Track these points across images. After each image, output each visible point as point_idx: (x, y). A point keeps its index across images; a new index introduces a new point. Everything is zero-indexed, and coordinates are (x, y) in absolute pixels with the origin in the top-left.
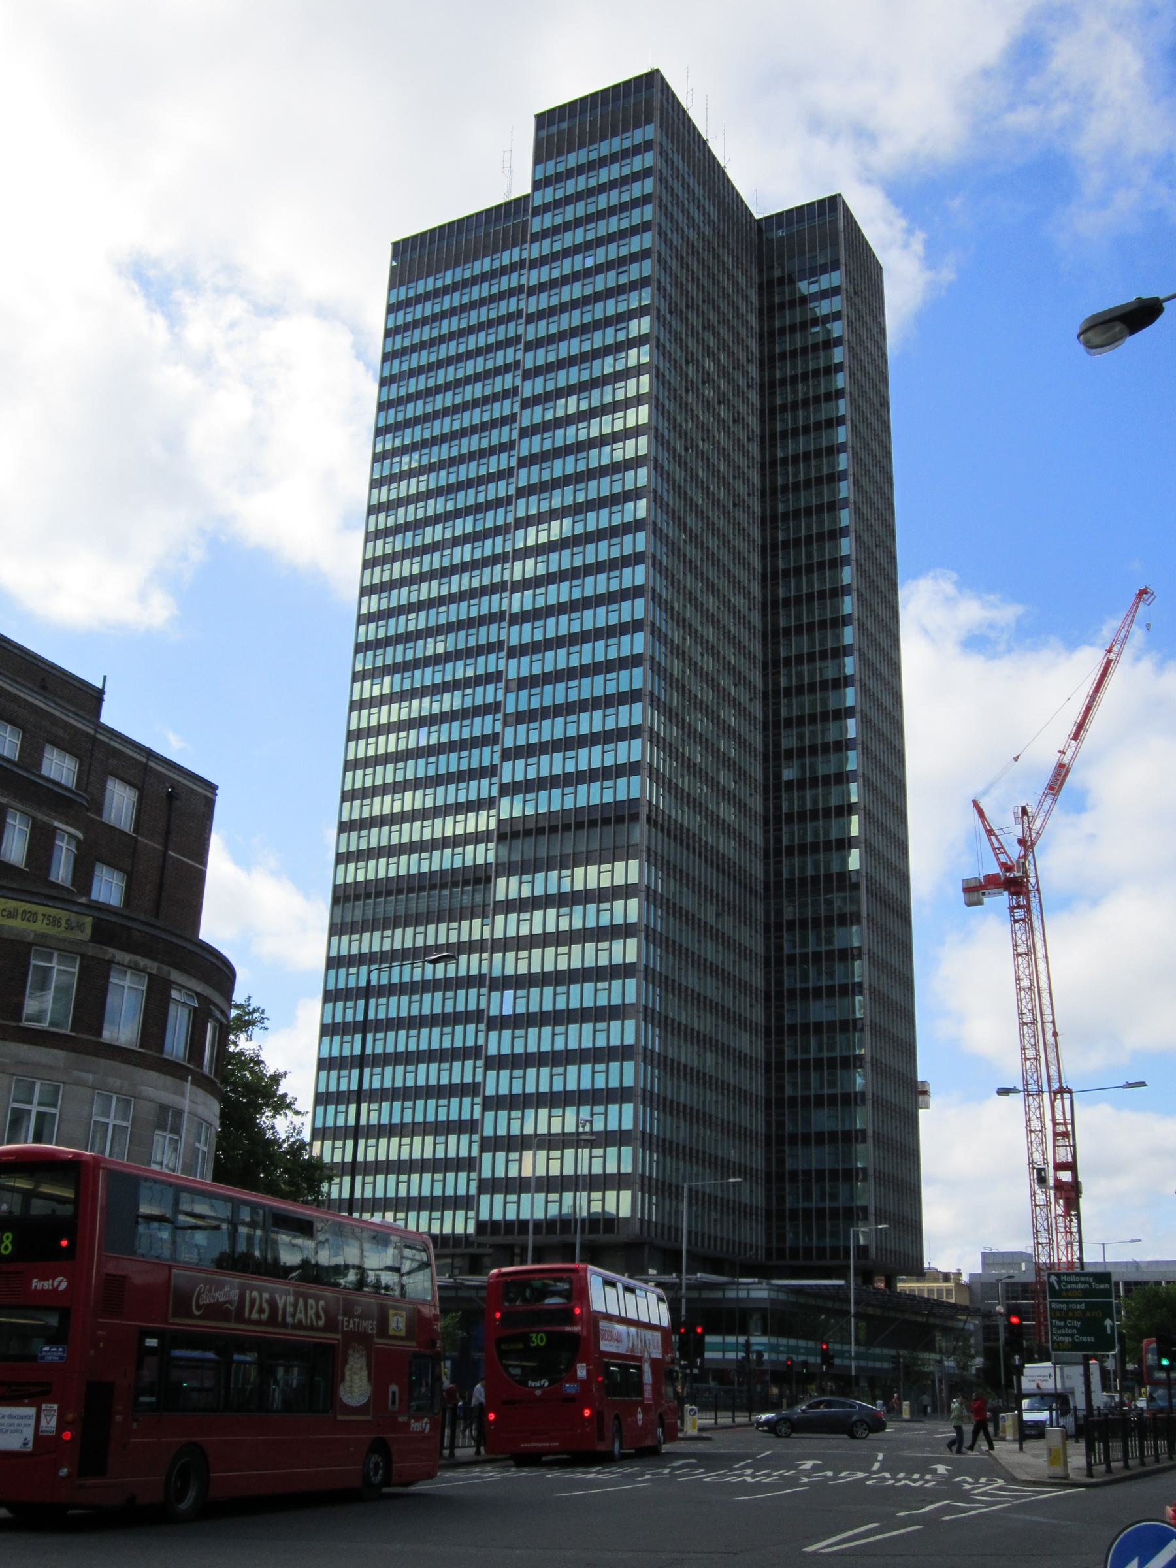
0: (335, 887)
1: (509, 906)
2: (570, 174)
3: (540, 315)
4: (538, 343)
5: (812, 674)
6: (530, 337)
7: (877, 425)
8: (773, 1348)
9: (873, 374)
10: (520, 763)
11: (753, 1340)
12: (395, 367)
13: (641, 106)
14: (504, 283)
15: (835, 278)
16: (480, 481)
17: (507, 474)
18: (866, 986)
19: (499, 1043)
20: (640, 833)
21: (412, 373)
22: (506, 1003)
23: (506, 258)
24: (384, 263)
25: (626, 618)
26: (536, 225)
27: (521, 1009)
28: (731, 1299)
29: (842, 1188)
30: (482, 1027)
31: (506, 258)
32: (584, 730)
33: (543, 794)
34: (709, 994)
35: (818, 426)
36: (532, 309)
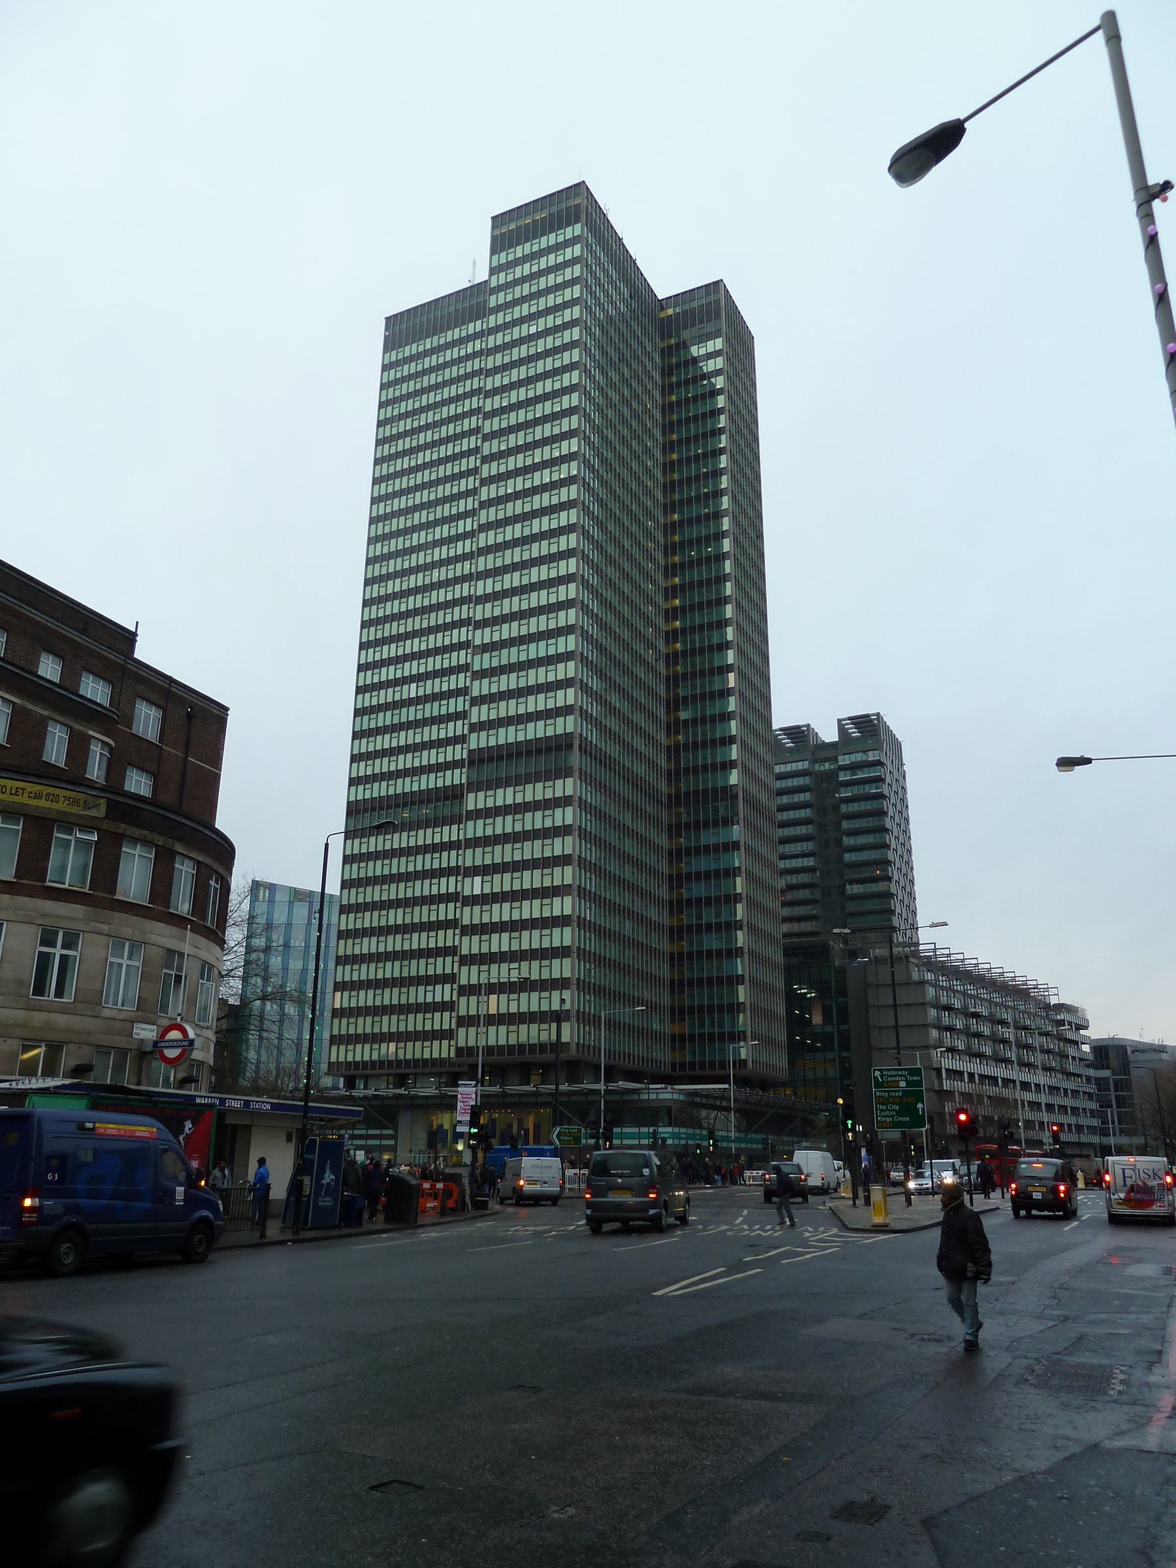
0: (349, 803)
1: (477, 814)
2: (518, 262)
3: (495, 391)
4: (494, 413)
5: (702, 641)
6: (488, 408)
7: (754, 555)
8: (675, 1136)
9: (747, 417)
10: (483, 734)
11: (661, 1130)
12: (383, 489)
13: (573, 208)
14: (469, 367)
15: (718, 344)
16: (458, 398)
17: (472, 513)
18: (743, 869)
19: (471, 945)
21: (401, 417)
22: (476, 886)
23: (471, 328)
24: (379, 333)
25: (562, 598)
26: (493, 302)
27: (487, 890)
29: (727, 1018)
30: (458, 905)
31: (471, 328)
32: (531, 709)
33: (498, 848)
34: (627, 877)
35: (705, 435)
36: (489, 387)
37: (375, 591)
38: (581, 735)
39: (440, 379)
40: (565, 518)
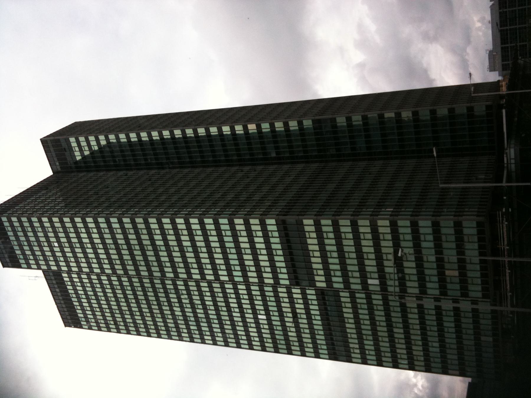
17: (235, 285)
20: (291, 219)
24: (67, 328)
28: (516, 166)
37: (296, 347)
38: (278, 215)
39: (155, 303)
40: (256, 227)
